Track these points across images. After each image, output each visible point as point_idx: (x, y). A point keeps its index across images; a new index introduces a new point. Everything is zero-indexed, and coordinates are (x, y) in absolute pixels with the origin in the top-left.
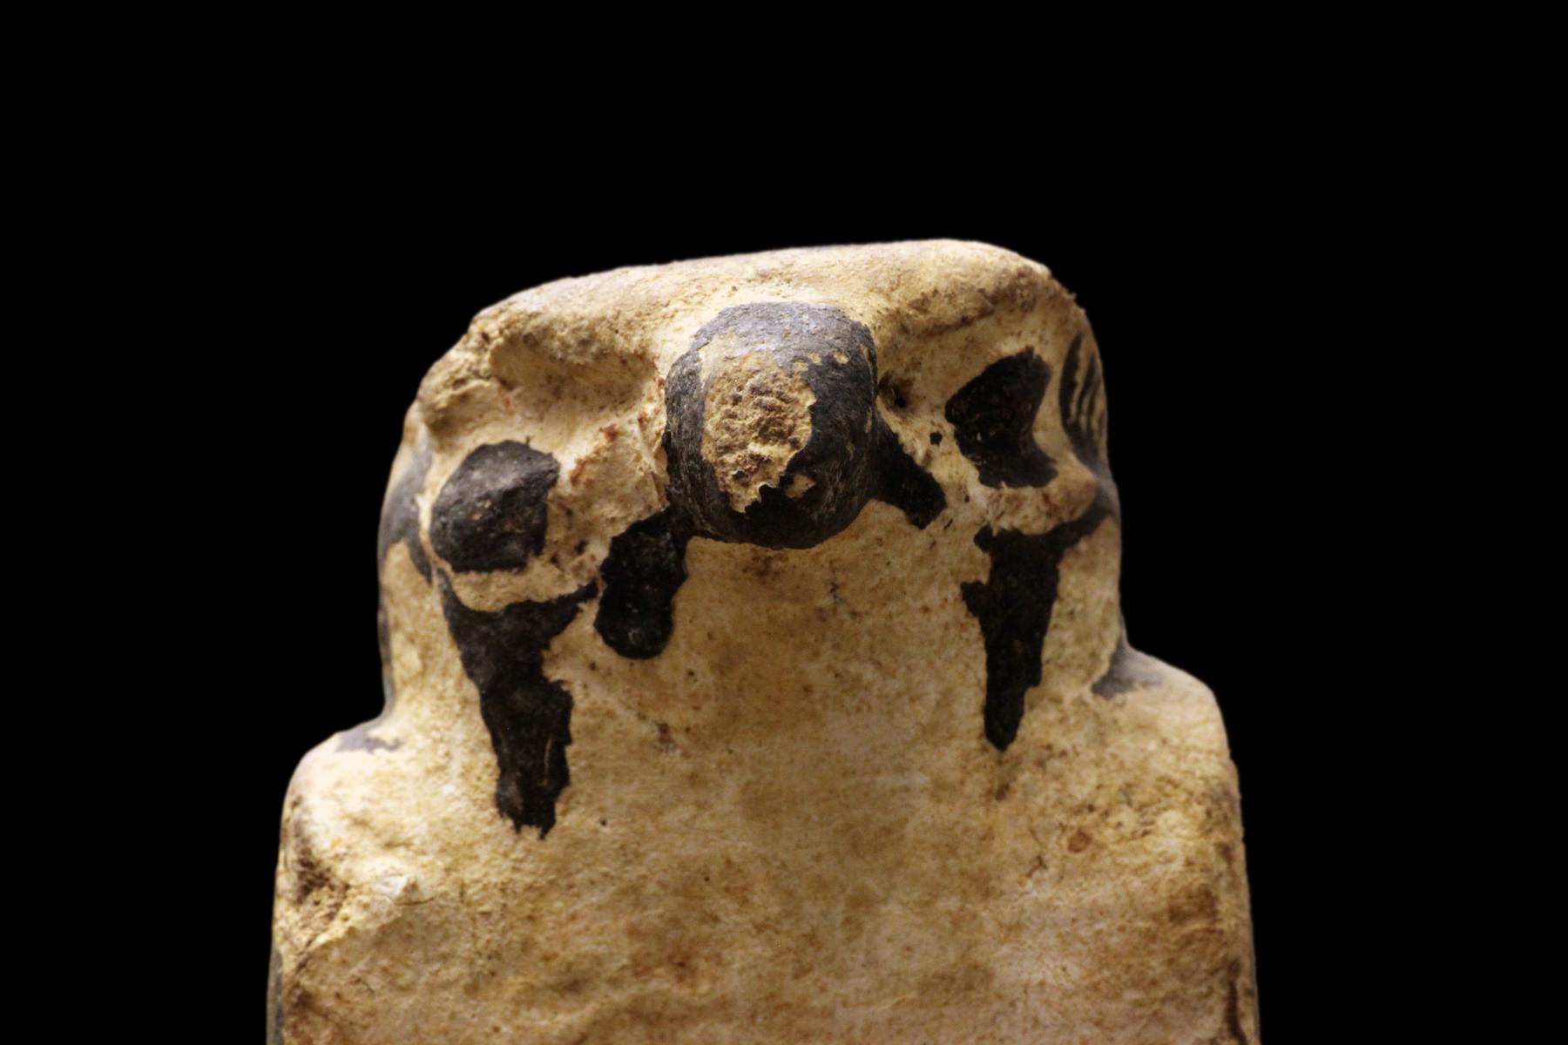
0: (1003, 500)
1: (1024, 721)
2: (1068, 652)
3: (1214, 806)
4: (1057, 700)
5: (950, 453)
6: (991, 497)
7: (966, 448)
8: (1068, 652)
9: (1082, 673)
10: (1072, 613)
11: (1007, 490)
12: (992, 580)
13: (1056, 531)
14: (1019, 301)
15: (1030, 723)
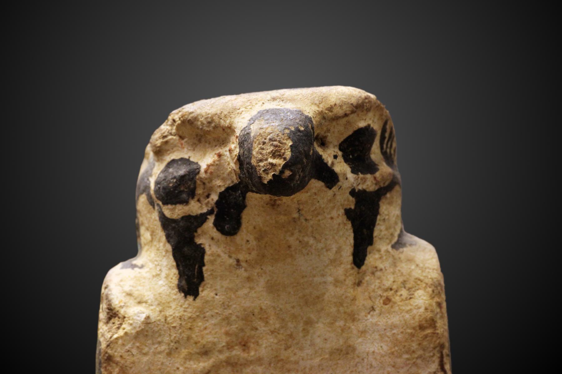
0: (359, 179)
1: (367, 258)
2: (383, 233)
3: (435, 289)
4: (379, 251)
5: (340, 162)
6: (355, 178)
7: (346, 160)
8: (383, 233)
9: (388, 241)
10: (384, 219)
11: (361, 175)
12: (355, 208)
13: (378, 190)
14: (365, 108)
15: (369, 259)
